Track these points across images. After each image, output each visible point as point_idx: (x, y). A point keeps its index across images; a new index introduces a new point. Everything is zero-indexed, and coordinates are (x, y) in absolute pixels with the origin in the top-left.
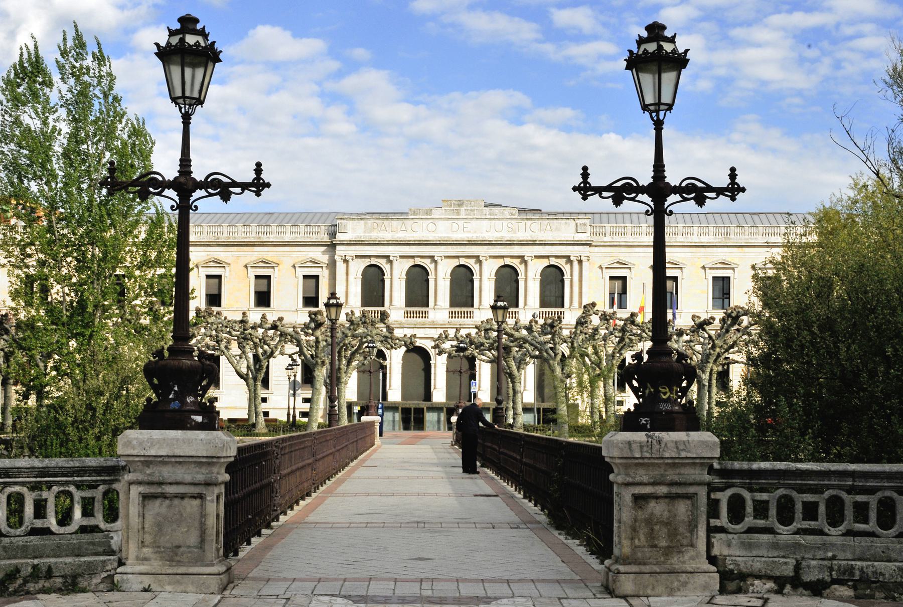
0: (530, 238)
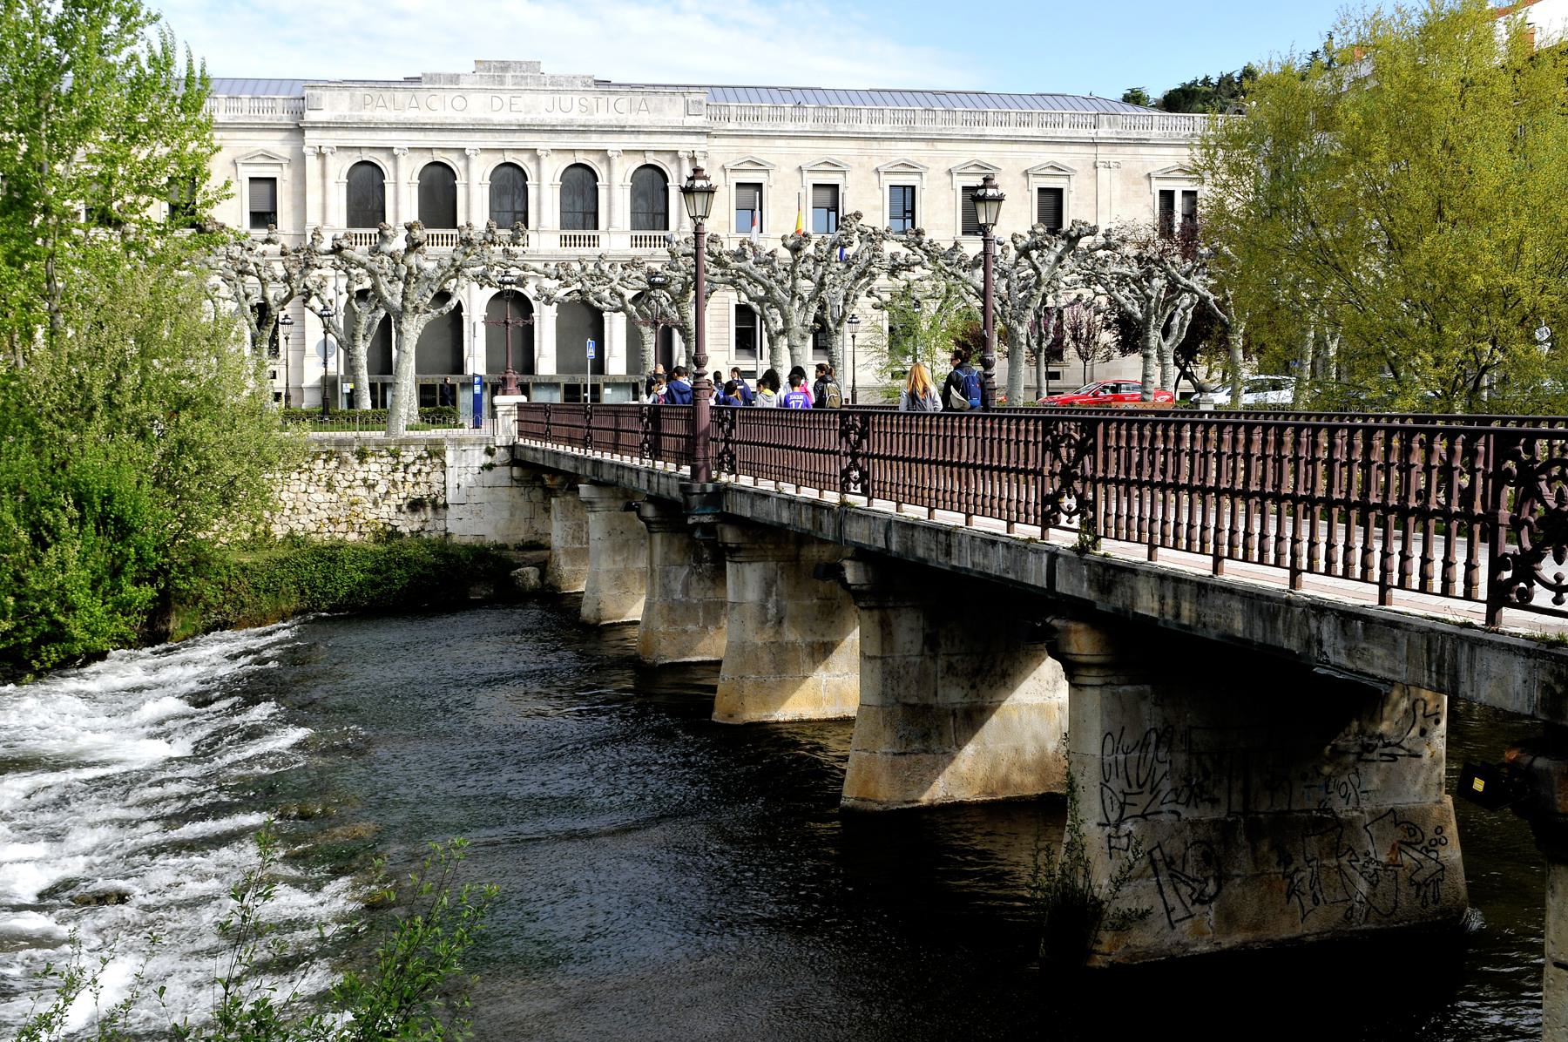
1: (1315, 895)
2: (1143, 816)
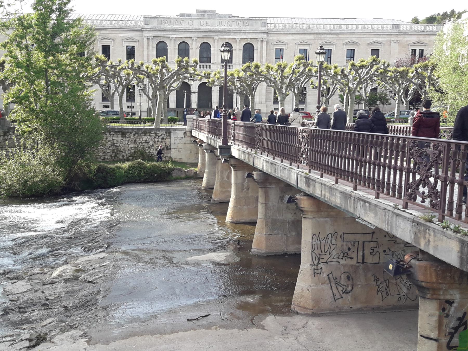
0: (238, 29)
1: (387, 292)
2: (326, 262)
